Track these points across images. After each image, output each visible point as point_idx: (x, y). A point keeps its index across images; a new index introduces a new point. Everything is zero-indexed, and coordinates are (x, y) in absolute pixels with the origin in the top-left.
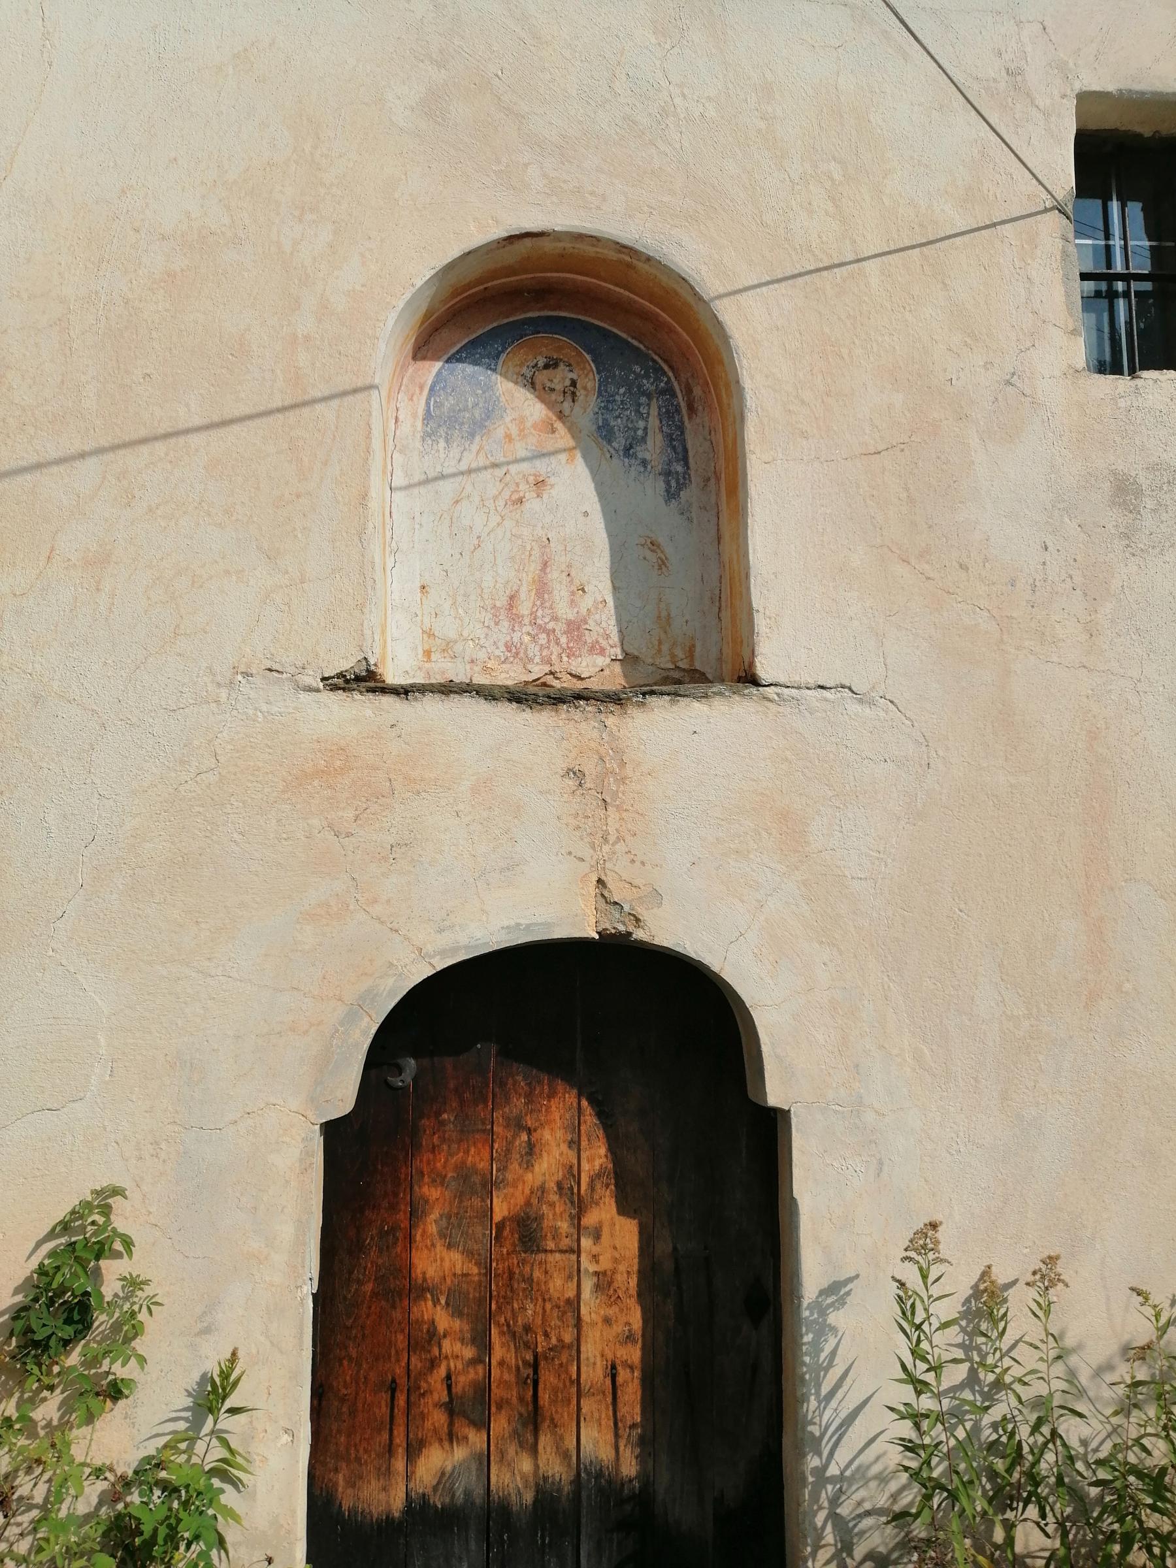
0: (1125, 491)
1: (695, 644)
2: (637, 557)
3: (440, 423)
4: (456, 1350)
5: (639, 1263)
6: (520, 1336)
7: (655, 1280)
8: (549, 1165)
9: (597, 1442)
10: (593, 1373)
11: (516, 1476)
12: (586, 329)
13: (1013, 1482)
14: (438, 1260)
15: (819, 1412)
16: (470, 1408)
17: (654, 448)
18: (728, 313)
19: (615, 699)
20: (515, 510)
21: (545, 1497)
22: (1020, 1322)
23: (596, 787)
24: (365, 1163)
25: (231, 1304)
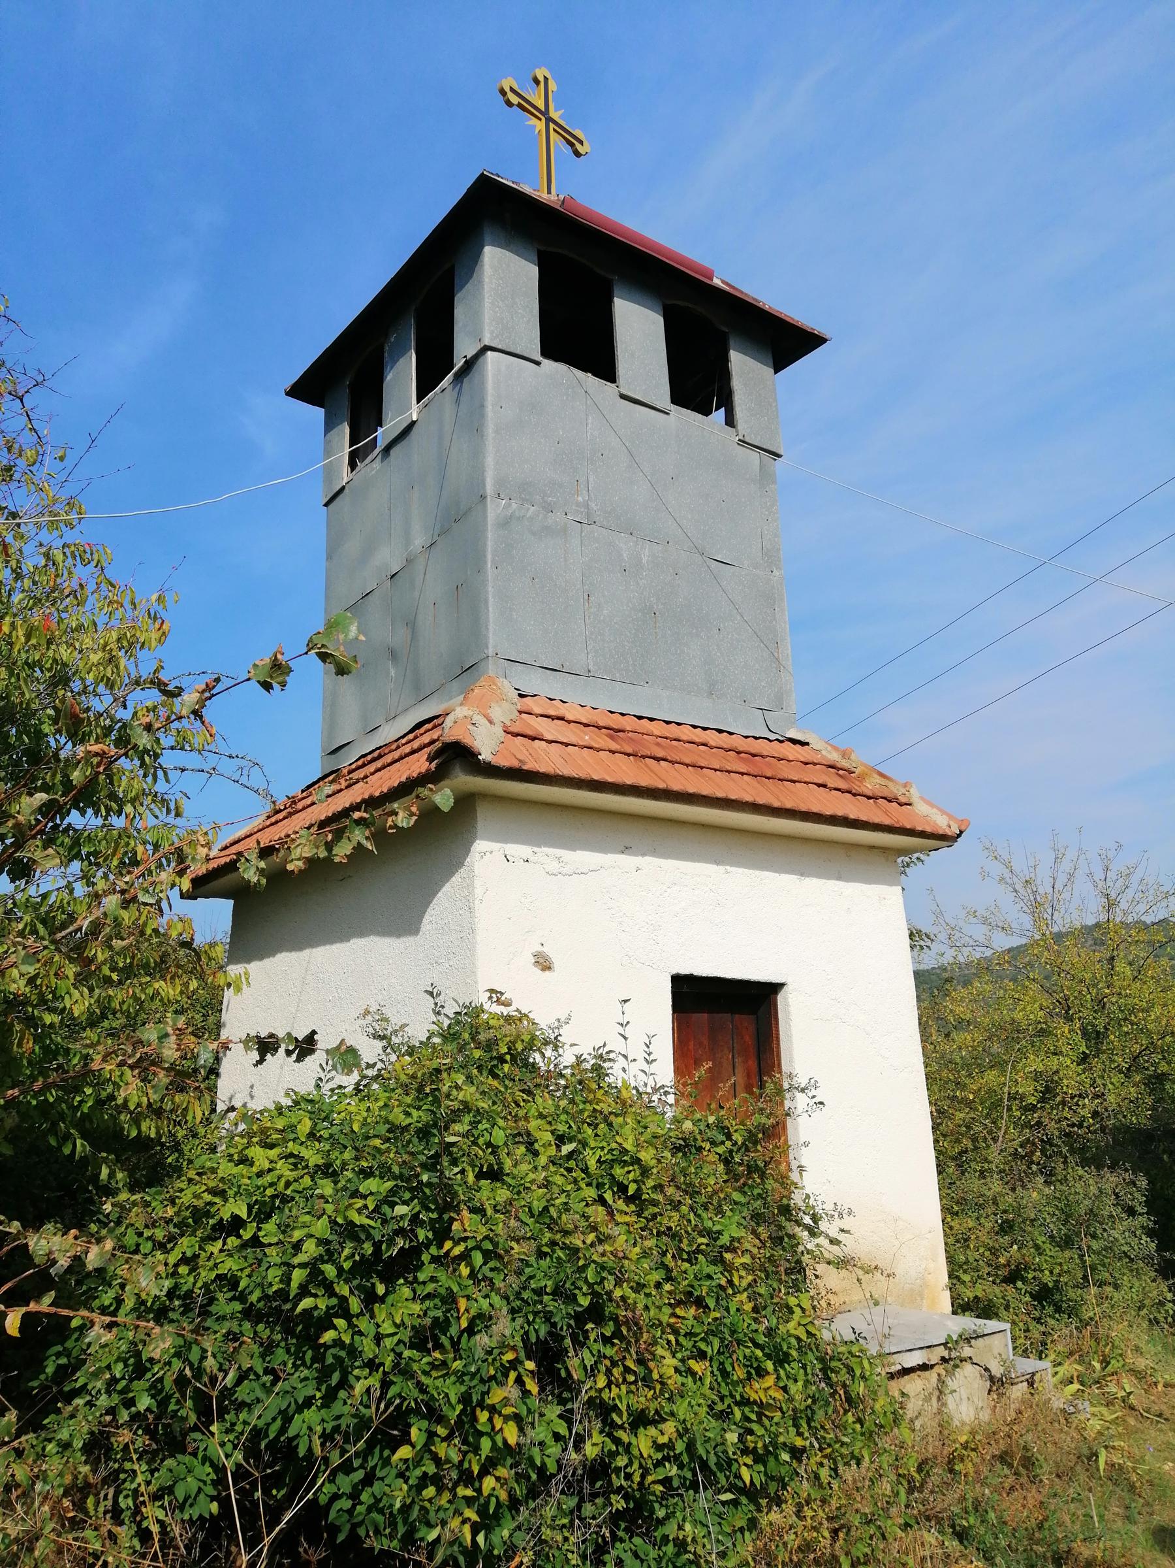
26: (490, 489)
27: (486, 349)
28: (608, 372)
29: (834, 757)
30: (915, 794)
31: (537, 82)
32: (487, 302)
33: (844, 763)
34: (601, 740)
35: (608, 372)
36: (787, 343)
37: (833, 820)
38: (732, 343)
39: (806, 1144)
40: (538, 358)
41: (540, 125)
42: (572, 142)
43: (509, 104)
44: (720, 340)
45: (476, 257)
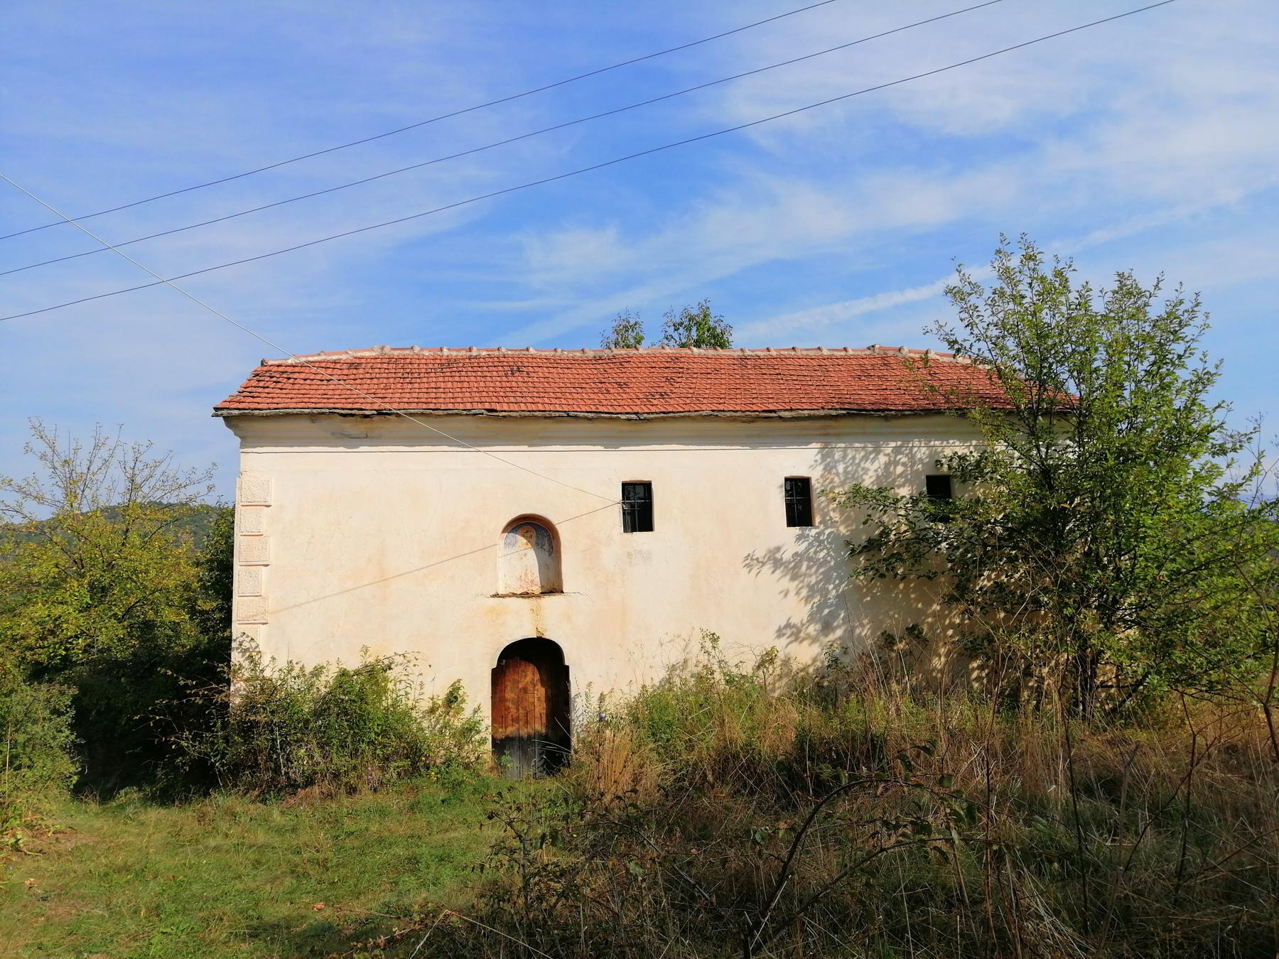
0: (629, 555)
1: (553, 587)
2: (543, 568)
3: (507, 545)
4: (513, 711)
6: (525, 708)
7: (548, 699)
8: (529, 678)
10: (537, 715)
11: (524, 732)
12: (535, 529)
14: (510, 695)
17: (546, 546)
18: (558, 527)
19: (538, 596)
20: (522, 560)
24: (498, 676)
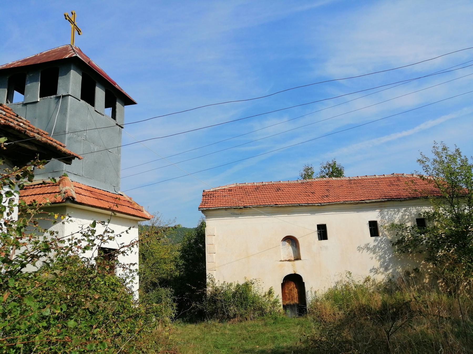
0: (321, 248)
1: (298, 258)
2: (294, 252)
3: (283, 245)
4: (288, 296)
5: (290, 348)
9: (296, 301)
11: (292, 303)
13: (317, 301)
14: (287, 291)
15: (307, 297)
16: (289, 299)
19: (293, 261)
20: (288, 250)
21: (293, 304)
22: (317, 293)
23: (293, 266)
24: (283, 285)
25: (278, 292)
26: (67, 130)
27: (69, 95)
28: (93, 104)
29: (128, 199)
30: (144, 209)
31: (72, 14)
32: (71, 84)
33: (130, 201)
34: (88, 194)
35: (93, 104)
36: (128, 101)
37: (134, 215)
38: (117, 100)
39: (245, 278)
40: (80, 99)
41: (73, 26)
42: (79, 32)
43: (66, 19)
44: (116, 97)
45: (68, 71)
